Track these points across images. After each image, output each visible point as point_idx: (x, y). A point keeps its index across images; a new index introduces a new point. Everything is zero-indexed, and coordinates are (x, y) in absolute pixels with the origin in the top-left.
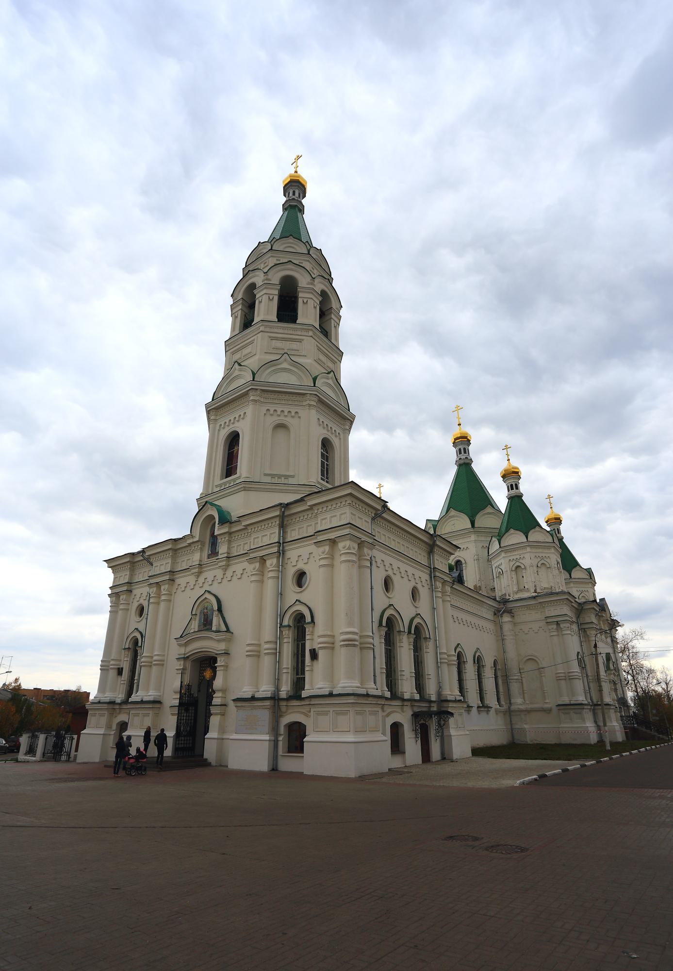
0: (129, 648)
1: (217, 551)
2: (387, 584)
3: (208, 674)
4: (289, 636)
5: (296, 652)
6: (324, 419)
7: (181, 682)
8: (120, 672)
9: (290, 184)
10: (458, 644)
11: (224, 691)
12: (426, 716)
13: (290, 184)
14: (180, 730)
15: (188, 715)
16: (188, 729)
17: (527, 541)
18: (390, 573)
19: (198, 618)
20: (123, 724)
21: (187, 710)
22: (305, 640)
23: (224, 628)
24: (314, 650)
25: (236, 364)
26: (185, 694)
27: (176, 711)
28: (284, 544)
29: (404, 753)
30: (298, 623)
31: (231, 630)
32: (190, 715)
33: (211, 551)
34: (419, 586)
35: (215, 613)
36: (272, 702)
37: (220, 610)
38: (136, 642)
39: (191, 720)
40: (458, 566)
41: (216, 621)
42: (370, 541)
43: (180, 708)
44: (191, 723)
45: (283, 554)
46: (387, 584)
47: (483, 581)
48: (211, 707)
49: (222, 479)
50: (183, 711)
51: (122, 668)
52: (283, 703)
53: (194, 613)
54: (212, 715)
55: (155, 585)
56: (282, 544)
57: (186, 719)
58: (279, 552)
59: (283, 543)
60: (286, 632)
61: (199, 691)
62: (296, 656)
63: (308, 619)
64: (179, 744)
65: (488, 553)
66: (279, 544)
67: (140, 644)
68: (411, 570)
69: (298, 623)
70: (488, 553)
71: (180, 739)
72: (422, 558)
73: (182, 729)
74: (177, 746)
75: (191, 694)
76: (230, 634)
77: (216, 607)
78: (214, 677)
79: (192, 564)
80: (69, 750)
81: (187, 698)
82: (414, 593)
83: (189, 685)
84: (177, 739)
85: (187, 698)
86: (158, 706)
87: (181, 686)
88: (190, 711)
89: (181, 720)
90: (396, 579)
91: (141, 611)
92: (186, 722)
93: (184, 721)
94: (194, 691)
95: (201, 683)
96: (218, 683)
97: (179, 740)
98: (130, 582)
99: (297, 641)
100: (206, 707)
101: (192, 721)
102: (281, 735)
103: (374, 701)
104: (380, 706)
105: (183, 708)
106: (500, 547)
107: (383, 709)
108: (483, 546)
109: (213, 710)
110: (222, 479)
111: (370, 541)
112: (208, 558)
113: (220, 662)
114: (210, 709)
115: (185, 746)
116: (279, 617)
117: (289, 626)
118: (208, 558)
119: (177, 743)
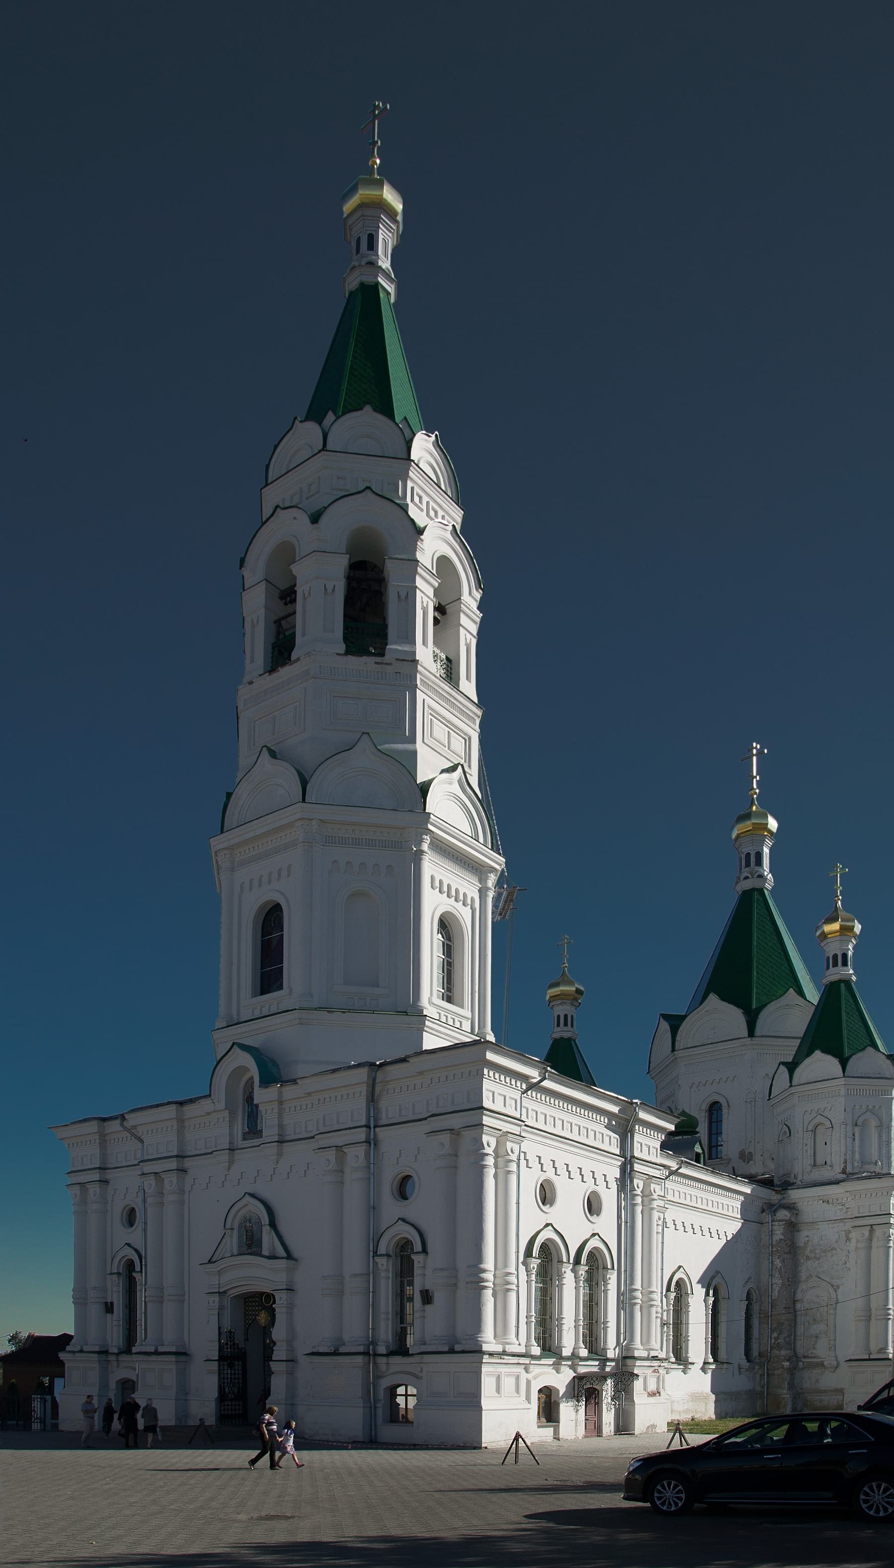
0: (119, 1274)
1: (259, 1128)
2: (546, 1195)
3: (263, 1318)
4: (386, 1267)
5: (399, 1291)
6: (442, 874)
7: (219, 1328)
8: (109, 1308)
9: (362, 218)
10: (680, 1267)
11: (290, 1342)
12: (595, 1379)
13: (362, 218)
14: (224, 1391)
15: (233, 1372)
16: (236, 1390)
17: (844, 1076)
18: (550, 1174)
19: (235, 1234)
20: (125, 1382)
21: (231, 1366)
22: (413, 1276)
23: (281, 1252)
24: (427, 1291)
25: (265, 749)
26: (227, 1344)
27: (215, 1366)
28: (377, 1129)
29: (558, 1422)
30: (401, 1251)
31: (296, 1253)
32: (237, 1372)
33: (248, 1127)
34: (601, 1189)
35: (266, 1229)
36: (366, 1358)
37: (273, 1224)
38: (130, 1265)
39: (238, 1378)
40: (715, 1112)
41: (268, 1239)
42: (516, 1130)
43: (222, 1363)
44: (238, 1383)
45: (375, 1144)
46: (546, 1195)
47: (758, 1143)
48: (271, 1363)
49: (254, 995)
50: (226, 1367)
51: (112, 1303)
52: (382, 1360)
53: (228, 1226)
54: (273, 1373)
55: (152, 1177)
56: (372, 1129)
57: (231, 1378)
58: (368, 1142)
59: (375, 1127)
60: (382, 1262)
61: (247, 1339)
62: (399, 1298)
63: (418, 1247)
64: (224, 1410)
65: (770, 1096)
66: (368, 1129)
67: (138, 1268)
68: (588, 1166)
69: (401, 1251)
70: (770, 1096)
71: (226, 1403)
72: (611, 1140)
73: (227, 1390)
74: (223, 1413)
75: (234, 1344)
76: (292, 1262)
77: (265, 1220)
78: (272, 1321)
79: (216, 1147)
80: (43, 1417)
81: (229, 1350)
82: (593, 1206)
83: (230, 1332)
84: (222, 1404)
85: (229, 1350)
86: (183, 1358)
87: (220, 1334)
88: (236, 1367)
89: (224, 1378)
90: (561, 1184)
91: (130, 1217)
92: (231, 1381)
93: (229, 1380)
94: (239, 1338)
95: (248, 1329)
96: (278, 1333)
97: (224, 1405)
98: (103, 1166)
99: (401, 1277)
100: (264, 1363)
101: (241, 1381)
102: (380, 1400)
103: (515, 1360)
104: (523, 1366)
105: (226, 1363)
106: (791, 1086)
107: (527, 1370)
108: (767, 1075)
109: (274, 1366)
110: (254, 995)
111: (516, 1130)
112: (244, 1139)
113: (281, 1299)
114: (269, 1365)
115: (234, 1412)
116: (371, 1242)
117: (388, 1255)
118: (244, 1139)
119: (222, 1408)
